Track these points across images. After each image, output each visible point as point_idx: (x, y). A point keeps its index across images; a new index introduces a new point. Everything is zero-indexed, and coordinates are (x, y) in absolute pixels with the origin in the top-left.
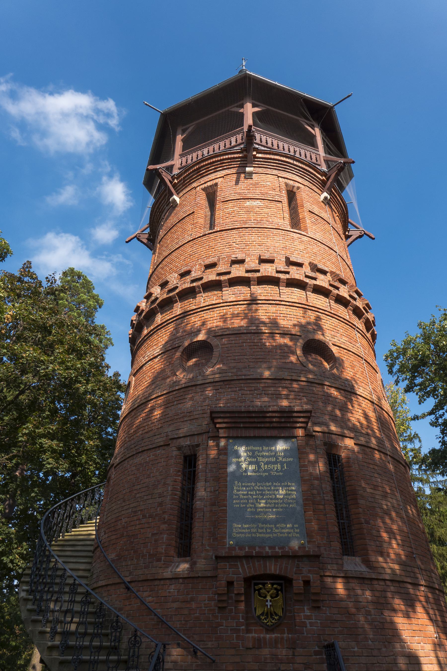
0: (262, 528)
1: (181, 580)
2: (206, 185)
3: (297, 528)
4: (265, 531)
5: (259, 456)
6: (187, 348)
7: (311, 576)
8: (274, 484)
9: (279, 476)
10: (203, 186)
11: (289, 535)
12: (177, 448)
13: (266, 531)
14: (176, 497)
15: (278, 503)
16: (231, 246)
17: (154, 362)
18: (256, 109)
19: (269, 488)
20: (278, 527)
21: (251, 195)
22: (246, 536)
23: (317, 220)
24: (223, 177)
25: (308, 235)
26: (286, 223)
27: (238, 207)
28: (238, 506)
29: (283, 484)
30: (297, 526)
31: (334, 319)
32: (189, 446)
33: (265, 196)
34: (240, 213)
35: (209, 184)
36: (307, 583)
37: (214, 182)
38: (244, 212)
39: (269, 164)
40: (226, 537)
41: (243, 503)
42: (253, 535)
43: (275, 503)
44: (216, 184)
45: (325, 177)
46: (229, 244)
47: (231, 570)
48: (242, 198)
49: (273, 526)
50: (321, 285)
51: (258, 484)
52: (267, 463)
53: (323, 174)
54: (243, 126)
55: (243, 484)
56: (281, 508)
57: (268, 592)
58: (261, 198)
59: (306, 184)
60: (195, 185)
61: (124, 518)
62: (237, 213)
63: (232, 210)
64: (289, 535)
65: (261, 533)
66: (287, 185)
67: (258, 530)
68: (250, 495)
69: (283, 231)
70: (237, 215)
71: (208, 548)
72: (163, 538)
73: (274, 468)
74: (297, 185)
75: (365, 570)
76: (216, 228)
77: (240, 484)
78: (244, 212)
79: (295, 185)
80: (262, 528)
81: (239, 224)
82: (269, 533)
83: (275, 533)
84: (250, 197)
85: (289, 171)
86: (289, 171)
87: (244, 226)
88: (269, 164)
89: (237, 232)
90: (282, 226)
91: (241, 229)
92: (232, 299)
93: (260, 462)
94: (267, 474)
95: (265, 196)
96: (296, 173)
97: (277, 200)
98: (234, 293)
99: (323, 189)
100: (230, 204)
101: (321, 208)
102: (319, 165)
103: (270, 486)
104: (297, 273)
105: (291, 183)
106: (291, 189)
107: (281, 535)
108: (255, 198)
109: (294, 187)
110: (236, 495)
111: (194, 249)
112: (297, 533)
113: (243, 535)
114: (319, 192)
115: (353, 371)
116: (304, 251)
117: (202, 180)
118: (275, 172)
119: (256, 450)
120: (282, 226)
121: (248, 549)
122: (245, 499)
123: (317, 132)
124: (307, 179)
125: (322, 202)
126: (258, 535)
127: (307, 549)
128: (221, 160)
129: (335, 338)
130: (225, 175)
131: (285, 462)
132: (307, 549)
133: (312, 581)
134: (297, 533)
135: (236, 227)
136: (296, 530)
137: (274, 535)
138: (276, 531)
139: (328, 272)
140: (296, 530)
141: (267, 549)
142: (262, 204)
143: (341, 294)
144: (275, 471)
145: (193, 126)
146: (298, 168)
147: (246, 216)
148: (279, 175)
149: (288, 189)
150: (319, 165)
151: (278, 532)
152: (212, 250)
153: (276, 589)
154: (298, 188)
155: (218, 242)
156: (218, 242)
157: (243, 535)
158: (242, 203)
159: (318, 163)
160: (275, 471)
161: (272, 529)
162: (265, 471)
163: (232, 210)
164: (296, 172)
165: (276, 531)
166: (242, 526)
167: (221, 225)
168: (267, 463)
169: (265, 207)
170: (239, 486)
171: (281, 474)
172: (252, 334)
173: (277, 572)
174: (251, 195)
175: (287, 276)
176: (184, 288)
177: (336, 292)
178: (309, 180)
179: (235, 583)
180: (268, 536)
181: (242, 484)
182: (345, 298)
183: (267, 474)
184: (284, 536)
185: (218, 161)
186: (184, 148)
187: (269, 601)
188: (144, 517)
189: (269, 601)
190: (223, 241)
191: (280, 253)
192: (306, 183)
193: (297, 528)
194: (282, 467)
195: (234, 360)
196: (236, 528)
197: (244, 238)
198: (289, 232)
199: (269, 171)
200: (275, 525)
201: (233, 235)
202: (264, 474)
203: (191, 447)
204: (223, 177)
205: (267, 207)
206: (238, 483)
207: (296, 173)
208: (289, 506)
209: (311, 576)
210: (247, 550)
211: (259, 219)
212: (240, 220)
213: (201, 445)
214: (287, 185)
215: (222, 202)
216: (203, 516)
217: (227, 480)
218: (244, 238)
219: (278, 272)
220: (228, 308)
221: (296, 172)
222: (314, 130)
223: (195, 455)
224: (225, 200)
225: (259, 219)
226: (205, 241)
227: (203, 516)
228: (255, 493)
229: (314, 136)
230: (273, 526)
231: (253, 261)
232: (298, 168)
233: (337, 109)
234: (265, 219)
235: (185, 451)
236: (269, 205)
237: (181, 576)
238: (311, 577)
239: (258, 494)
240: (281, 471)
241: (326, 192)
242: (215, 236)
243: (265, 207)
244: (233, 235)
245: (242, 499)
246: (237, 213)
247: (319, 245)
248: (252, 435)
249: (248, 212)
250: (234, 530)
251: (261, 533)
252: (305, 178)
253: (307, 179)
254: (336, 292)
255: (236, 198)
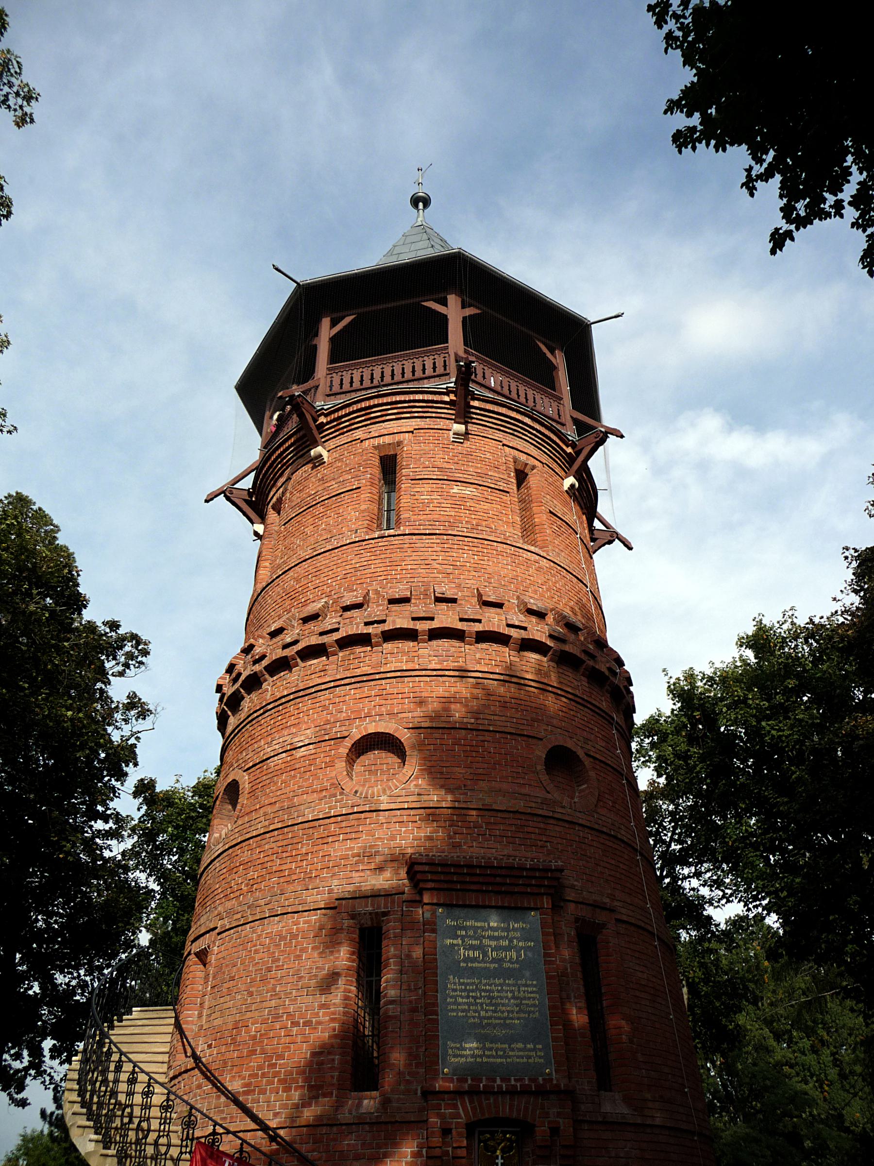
0: (490, 1049)
1: (367, 1128)
2: (381, 440)
3: (540, 1050)
4: (494, 1053)
5: (484, 937)
6: (359, 743)
7: (561, 1121)
8: (507, 982)
9: (515, 969)
10: (376, 442)
11: (529, 1061)
12: (349, 915)
13: (496, 1053)
14: (350, 994)
15: (512, 1012)
16: (428, 567)
17: (293, 757)
18: (469, 311)
19: (500, 988)
20: (513, 1049)
21: (461, 475)
22: (468, 1060)
23: (559, 527)
24: (412, 432)
25: (548, 558)
26: (514, 533)
27: (440, 493)
28: (455, 1014)
29: (519, 982)
30: (540, 1046)
31: (586, 709)
32: (370, 914)
33: (484, 479)
34: (443, 505)
35: (387, 440)
36: (555, 1130)
37: (397, 438)
38: (449, 506)
39: (490, 420)
40: (438, 1063)
41: (463, 1011)
42: (479, 1060)
43: (508, 1012)
44: (399, 443)
45: (573, 448)
46: (426, 562)
47: (447, 1111)
48: (446, 478)
49: (507, 1046)
50: (571, 651)
51: (484, 981)
52: (497, 949)
53: (573, 445)
54: (447, 343)
55: (461, 980)
56: (518, 1019)
57: (499, 1144)
58: (476, 482)
59: (544, 461)
60: (359, 434)
61: (252, 1024)
62: (439, 505)
63: (429, 497)
64: (529, 1061)
65: (488, 1057)
66: (515, 460)
67: (484, 1052)
68: (473, 997)
69: (513, 548)
70: (438, 509)
71: (408, 1078)
72: (333, 1060)
73: (506, 956)
74: (532, 462)
75: (628, 1112)
76: (402, 528)
77: (457, 980)
78: (449, 506)
79: (529, 462)
80: (490, 1049)
81: (442, 527)
82: (501, 1057)
83: (509, 1057)
84: (459, 479)
85: (520, 435)
86: (520, 435)
87: (450, 532)
88: (490, 420)
89: (438, 541)
90: (511, 539)
91: (445, 537)
92: (433, 666)
93: (485, 946)
94: (496, 965)
95: (484, 479)
96: (530, 440)
97: (501, 488)
98: (436, 653)
99: (568, 470)
100: (426, 487)
101: (566, 504)
102: (563, 425)
103: (500, 985)
104: (537, 630)
105: (523, 457)
106: (522, 469)
107: (518, 1060)
108: (467, 480)
109: (526, 464)
110: (451, 997)
111: (363, 560)
112: (540, 1057)
113: (463, 1060)
114: (562, 474)
115: (612, 799)
116: (544, 587)
117: (375, 429)
118: (499, 435)
119: (478, 927)
120: (511, 539)
121: (472, 1080)
122: (465, 1004)
123: (559, 360)
124: (546, 451)
125: (566, 491)
126: (485, 1060)
127: (555, 1082)
128: (410, 401)
129: (589, 743)
130: (415, 429)
131: (522, 948)
132: (555, 1082)
133: (562, 1128)
134: (540, 1057)
135: (438, 532)
136: (539, 1053)
137: (508, 1060)
138: (511, 1053)
139: (580, 629)
140: (539, 1053)
141: (498, 1082)
142: (479, 495)
143: (597, 667)
144: (508, 962)
145: (354, 316)
146: (534, 432)
147: (453, 514)
148: (505, 442)
149: (519, 467)
150: (563, 425)
151: (514, 1056)
152: (396, 568)
153: (509, 1139)
154: (533, 467)
155: (406, 554)
156: (406, 554)
157: (463, 1060)
158: (445, 485)
159: (563, 420)
160: (508, 962)
161: (504, 1050)
162: (494, 961)
163: (429, 497)
164: (530, 438)
165: (511, 1053)
166: (461, 1045)
167: (411, 523)
168: (497, 949)
169: (484, 500)
170: (455, 984)
171: (515, 965)
172: (468, 731)
173: (514, 1115)
174: (461, 475)
175: (523, 634)
176: (350, 633)
177: (591, 663)
178: (548, 453)
179: (454, 1131)
180: (499, 1060)
181: (459, 981)
182: (603, 673)
183: (496, 965)
184: (521, 1060)
185: (405, 402)
186: (334, 357)
187: (500, 1157)
188: (295, 1024)
189: (500, 1157)
190: (415, 554)
191: (509, 588)
192: (545, 459)
193: (540, 1050)
194: (519, 956)
195: (442, 773)
196: (452, 1048)
197: (450, 554)
198: (521, 551)
199: (490, 433)
200: (510, 1045)
201: (432, 545)
202: (492, 966)
203: (374, 916)
204: (412, 432)
205: (486, 500)
206: (454, 978)
207: (530, 440)
208: (529, 1015)
209: (561, 1121)
210: (470, 1082)
211: (474, 522)
212: (442, 519)
213: (392, 913)
214: (515, 460)
215: (412, 480)
216: (400, 1028)
217: (437, 973)
218: (450, 554)
219: (509, 625)
220: (428, 679)
221: (530, 438)
222: (552, 353)
223: (380, 929)
224: (418, 477)
225: (474, 522)
226: (383, 548)
227: (400, 1028)
228: (479, 994)
229: (553, 368)
230: (507, 1046)
231: (466, 598)
232: (534, 432)
233: (597, 332)
234: (484, 523)
235: (362, 921)
236: (489, 497)
237: (368, 1120)
238: (561, 1123)
239: (485, 997)
240: (517, 962)
241: (574, 476)
242: (400, 542)
243: (484, 500)
244: (432, 545)
245: (460, 1004)
246: (439, 505)
247: (564, 575)
248: (474, 903)
249: (455, 506)
250: (450, 1052)
251: (488, 1057)
252: (543, 449)
253: (546, 451)
254: (591, 663)
255: (435, 477)
